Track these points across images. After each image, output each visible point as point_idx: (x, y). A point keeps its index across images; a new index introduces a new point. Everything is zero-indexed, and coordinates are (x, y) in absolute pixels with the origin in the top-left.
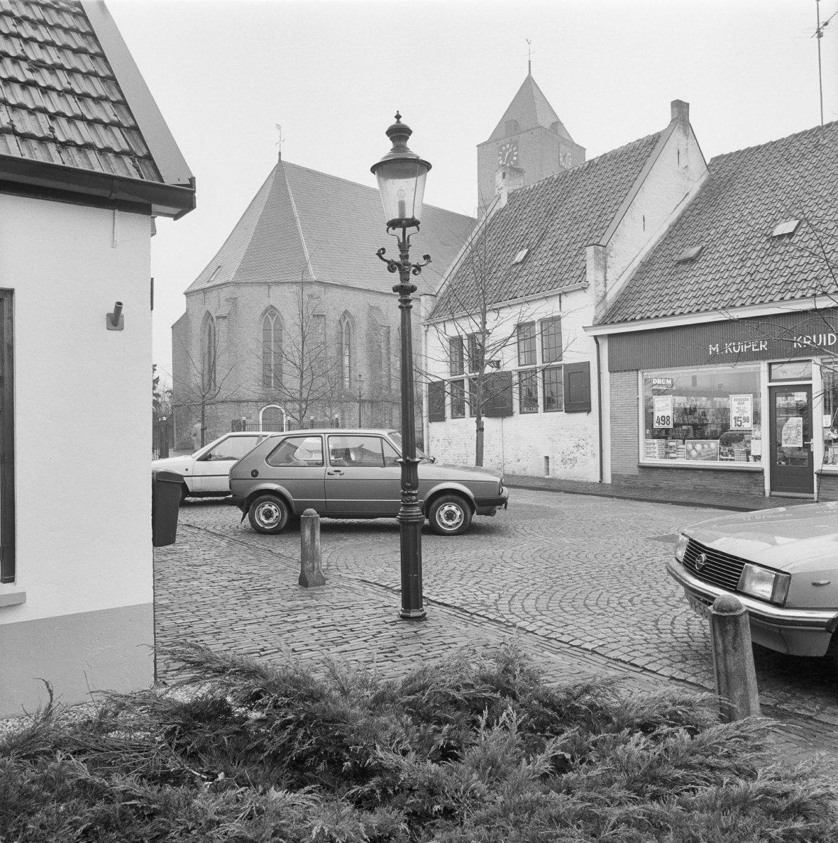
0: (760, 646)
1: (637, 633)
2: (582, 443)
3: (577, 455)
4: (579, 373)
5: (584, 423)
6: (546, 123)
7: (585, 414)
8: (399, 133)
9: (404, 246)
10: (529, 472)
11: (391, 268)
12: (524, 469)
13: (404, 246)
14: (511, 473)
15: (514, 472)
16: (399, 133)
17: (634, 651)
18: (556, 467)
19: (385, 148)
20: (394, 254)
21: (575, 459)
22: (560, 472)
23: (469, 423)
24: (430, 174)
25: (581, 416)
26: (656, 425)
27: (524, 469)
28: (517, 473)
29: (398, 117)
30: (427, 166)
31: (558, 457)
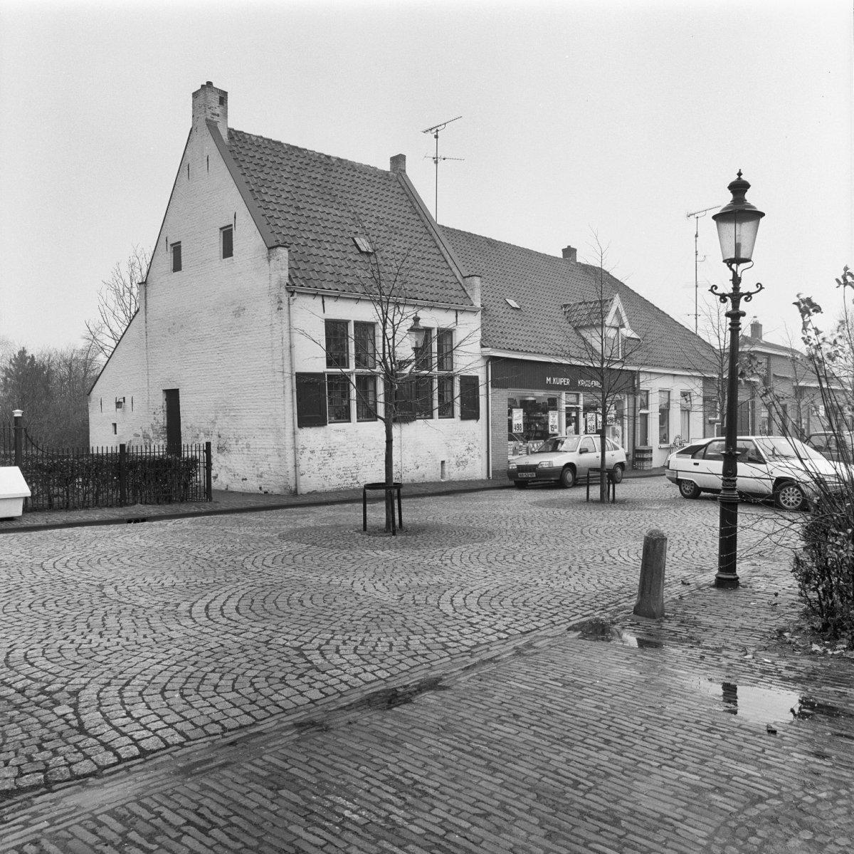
0: (643, 640)
1: (431, 641)
2: (471, 446)
3: (468, 457)
4: (470, 384)
5: (475, 429)
6: (403, 168)
7: (475, 421)
8: (739, 188)
9: (736, 280)
10: (428, 478)
11: (723, 298)
12: (424, 476)
13: (736, 280)
14: (410, 481)
15: (413, 480)
16: (739, 188)
17: (90, 658)
18: (451, 470)
19: (727, 198)
20: (727, 288)
21: (466, 461)
22: (454, 473)
23: (378, 428)
24: (762, 220)
25: (472, 423)
26: (514, 431)
27: (424, 476)
28: (417, 481)
29: (740, 174)
30: (762, 215)
31: (453, 460)
